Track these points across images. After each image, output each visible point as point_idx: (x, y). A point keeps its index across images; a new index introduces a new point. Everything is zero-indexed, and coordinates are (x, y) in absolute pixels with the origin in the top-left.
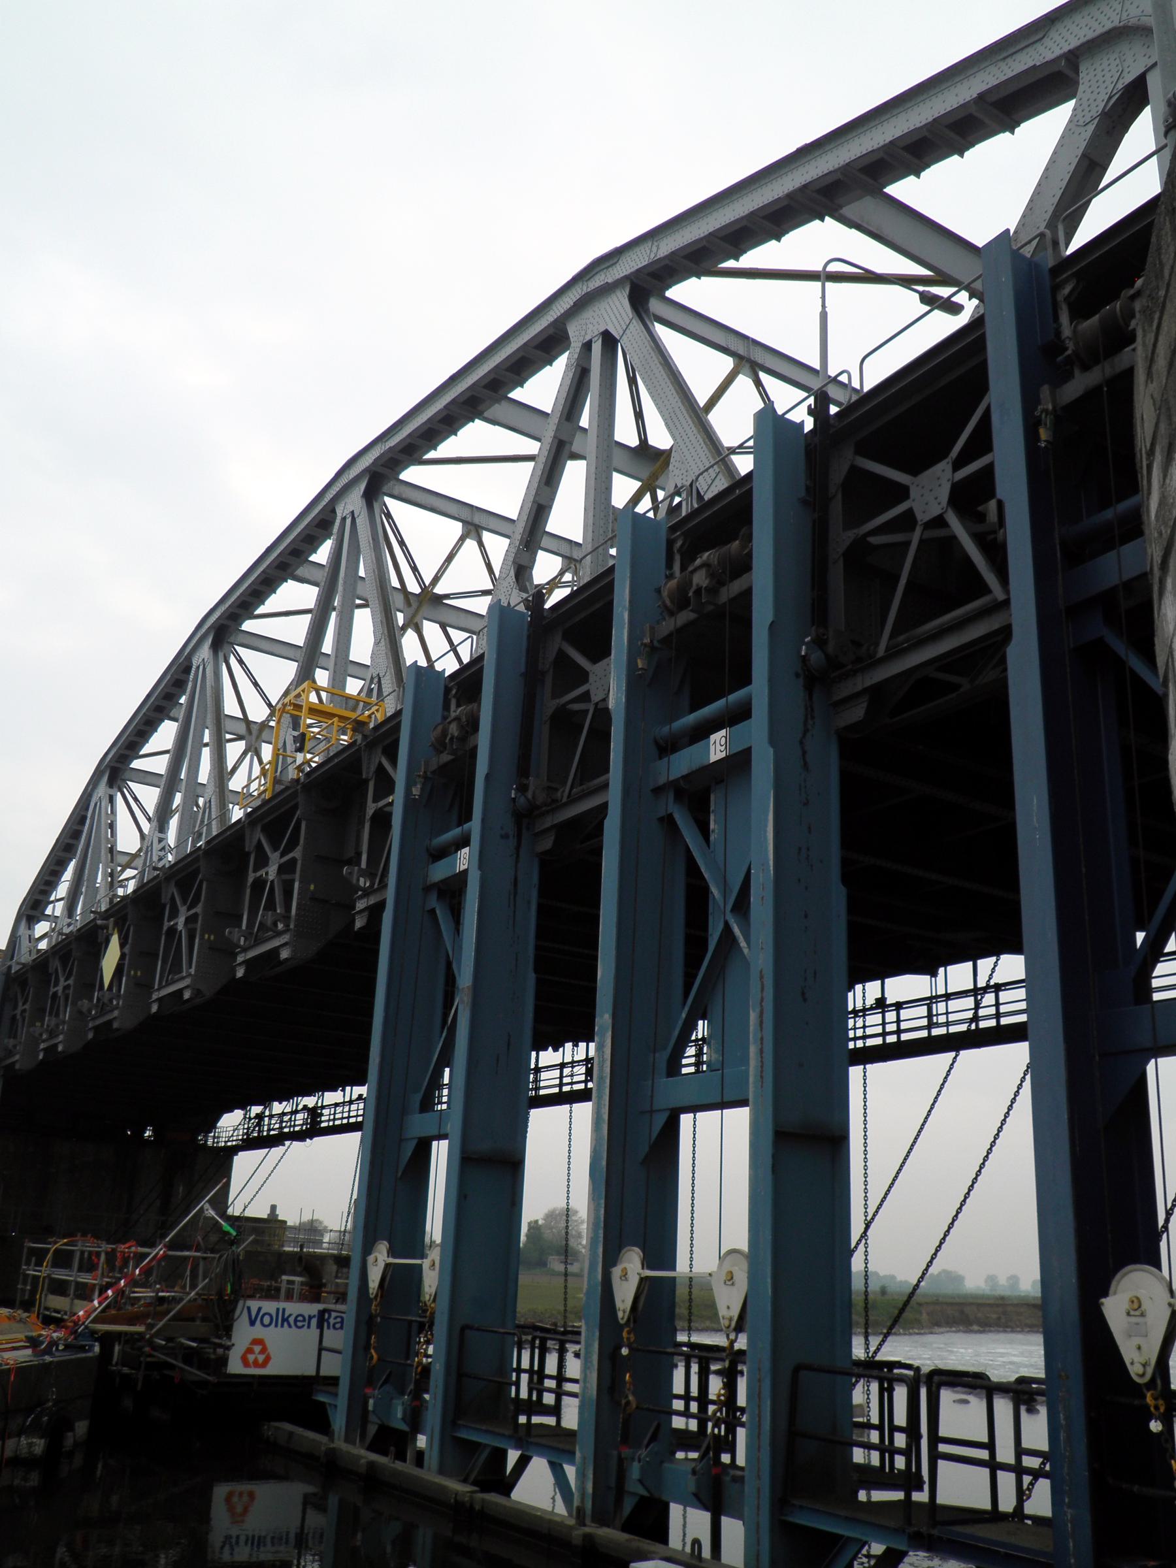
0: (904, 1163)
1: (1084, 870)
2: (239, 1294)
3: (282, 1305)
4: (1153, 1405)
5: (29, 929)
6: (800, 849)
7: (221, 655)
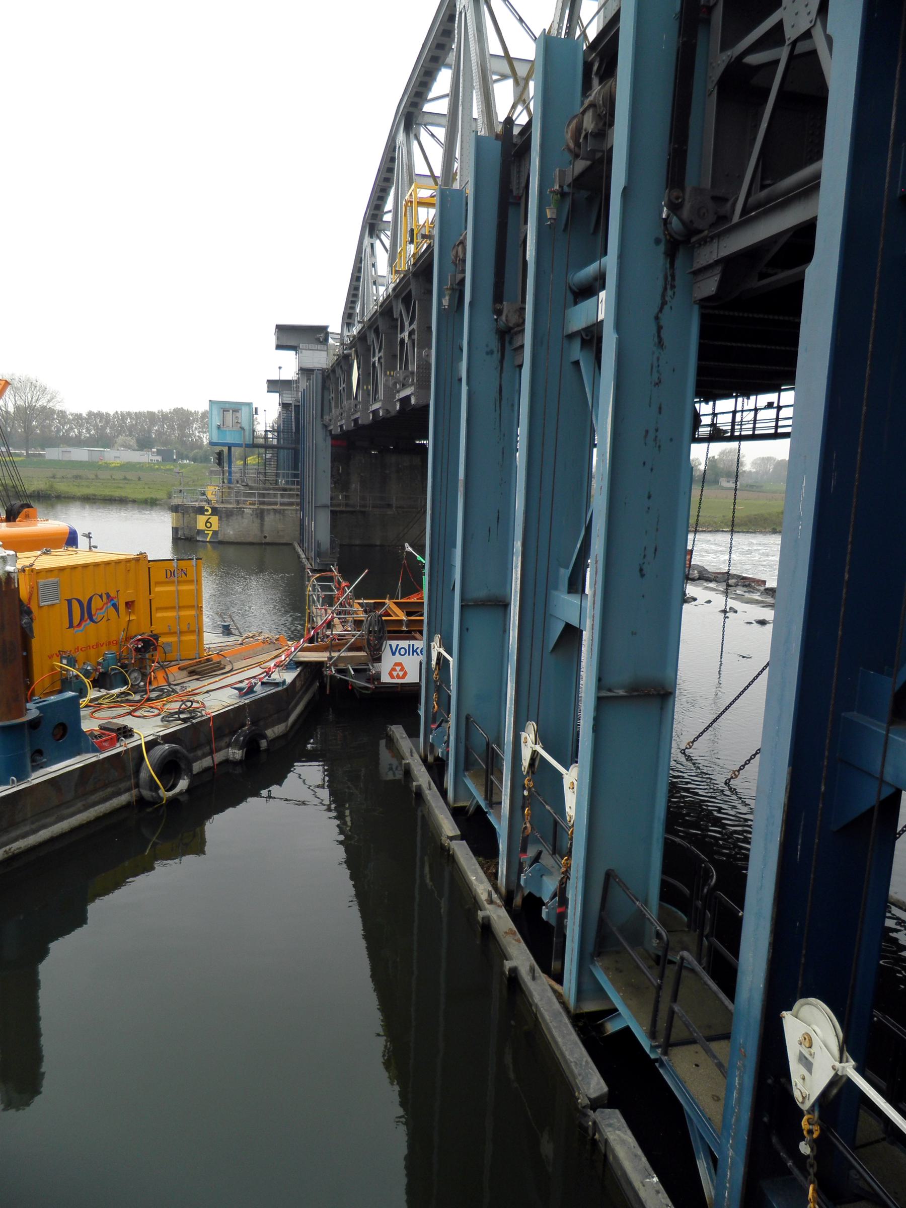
0: (748, 687)
1: (847, 576)
2: (381, 640)
3: (412, 642)
4: (806, 1129)
5: (349, 332)
6: (647, 432)
7: (412, 136)
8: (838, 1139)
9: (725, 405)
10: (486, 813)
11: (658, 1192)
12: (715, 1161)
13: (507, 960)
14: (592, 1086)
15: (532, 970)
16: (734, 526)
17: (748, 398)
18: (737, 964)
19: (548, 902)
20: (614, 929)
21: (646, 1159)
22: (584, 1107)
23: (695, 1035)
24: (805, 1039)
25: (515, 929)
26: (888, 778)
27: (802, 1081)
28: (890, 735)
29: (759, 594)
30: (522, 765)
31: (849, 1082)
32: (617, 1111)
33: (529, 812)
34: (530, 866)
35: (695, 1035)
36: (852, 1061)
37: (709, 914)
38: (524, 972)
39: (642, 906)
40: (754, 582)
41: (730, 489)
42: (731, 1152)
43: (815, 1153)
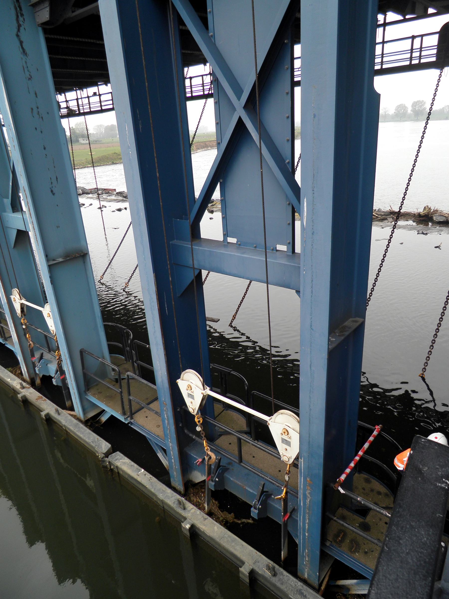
1: (158, 175)
6: (32, 109)
8: (209, 419)
9: (71, 95)
10: (5, 344)
11: (145, 475)
12: (165, 451)
13: (42, 412)
14: (103, 448)
15: (57, 411)
16: (93, 163)
17: (83, 91)
18: (153, 369)
19: (55, 376)
20: (92, 375)
21: (136, 465)
22: (102, 458)
23: (143, 405)
24: (189, 387)
25: (41, 395)
26: (196, 266)
27: (191, 404)
28: (193, 247)
29: (114, 196)
30: (17, 313)
31: (209, 396)
32: (118, 452)
33: (29, 336)
34: (39, 362)
35: (143, 405)
36: (208, 387)
37: (134, 352)
38: (53, 414)
39: (102, 360)
40: (110, 191)
41: (86, 144)
42: (170, 444)
43: (203, 428)
